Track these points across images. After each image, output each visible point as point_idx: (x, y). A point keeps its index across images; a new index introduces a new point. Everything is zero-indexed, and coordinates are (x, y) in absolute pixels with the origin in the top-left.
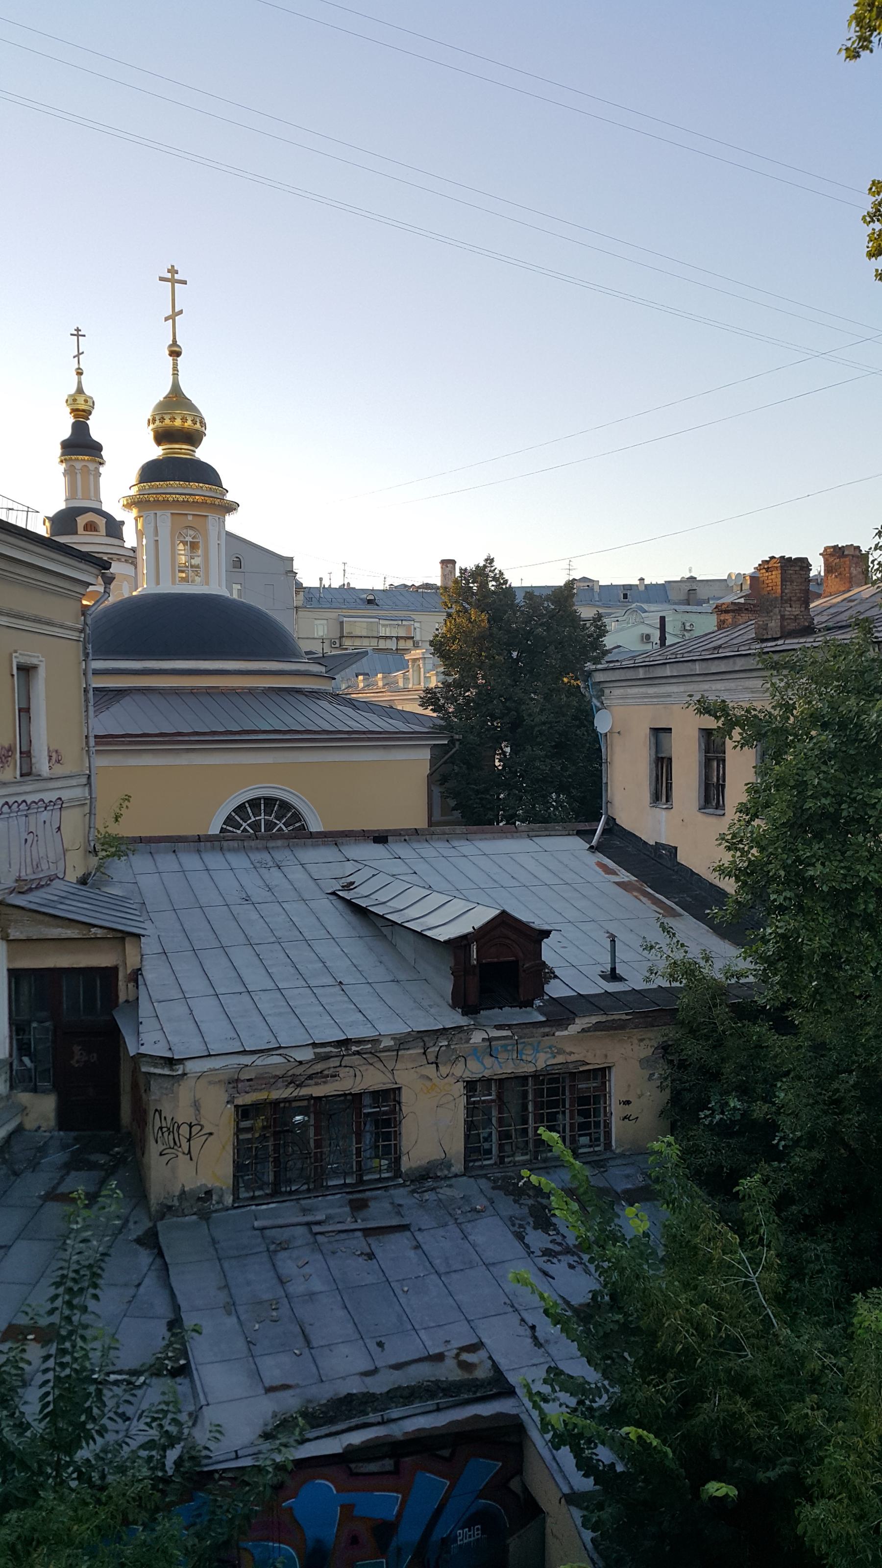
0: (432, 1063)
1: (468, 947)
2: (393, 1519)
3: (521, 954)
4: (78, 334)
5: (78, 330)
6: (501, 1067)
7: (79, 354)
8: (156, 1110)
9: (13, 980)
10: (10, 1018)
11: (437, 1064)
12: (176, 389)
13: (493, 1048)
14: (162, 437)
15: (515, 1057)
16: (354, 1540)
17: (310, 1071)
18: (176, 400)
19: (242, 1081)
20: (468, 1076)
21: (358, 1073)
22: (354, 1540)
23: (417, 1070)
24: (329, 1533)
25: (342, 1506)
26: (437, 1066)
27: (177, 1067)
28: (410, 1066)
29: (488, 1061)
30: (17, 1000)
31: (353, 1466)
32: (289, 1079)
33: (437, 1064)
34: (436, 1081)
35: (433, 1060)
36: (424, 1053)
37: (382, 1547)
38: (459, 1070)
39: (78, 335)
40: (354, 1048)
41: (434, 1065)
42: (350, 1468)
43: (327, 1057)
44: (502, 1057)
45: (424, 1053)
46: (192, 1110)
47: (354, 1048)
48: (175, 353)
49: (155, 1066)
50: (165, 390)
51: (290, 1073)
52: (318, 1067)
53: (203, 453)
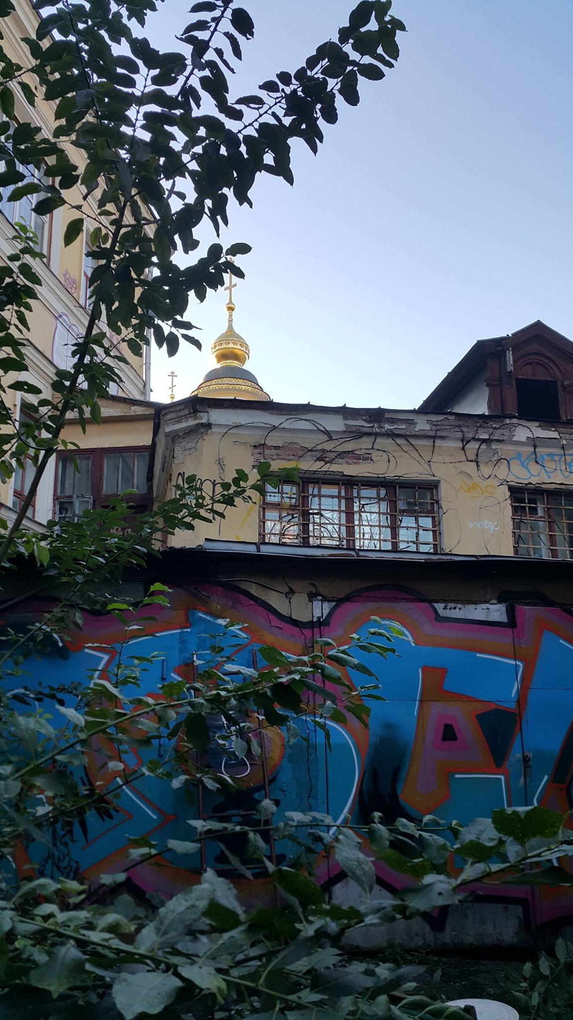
0: (472, 461)
1: (501, 355)
2: (512, 706)
3: (558, 374)
4: (173, 375)
5: (173, 373)
6: (549, 477)
7: (173, 386)
8: (180, 474)
9: (60, 465)
10: (55, 495)
11: (477, 462)
12: (230, 328)
13: (539, 456)
14: (222, 357)
15: (563, 468)
16: (449, 733)
17: (341, 449)
18: (230, 334)
19: (269, 448)
20: (513, 480)
21: (392, 459)
22: (449, 733)
23: (456, 465)
24: (405, 715)
25: (425, 669)
26: (478, 465)
27: (202, 414)
28: (448, 460)
29: (534, 468)
30: (63, 483)
31: (439, 606)
32: (318, 454)
33: (477, 462)
34: (477, 480)
35: (474, 458)
36: (463, 449)
37: (498, 754)
38: (502, 472)
39: (173, 376)
40: (387, 426)
41: (474, 464)
42: (435, 610)
43: (359, 434)
44: (550, 466)
45: (463, 449)
46: (216, 467)
47: (387, 426)
48: (231, 309)
49: (179, 422)
50: (224, 329)
51: (320, 447)
52: (349, 446)
53: (247, 366)
